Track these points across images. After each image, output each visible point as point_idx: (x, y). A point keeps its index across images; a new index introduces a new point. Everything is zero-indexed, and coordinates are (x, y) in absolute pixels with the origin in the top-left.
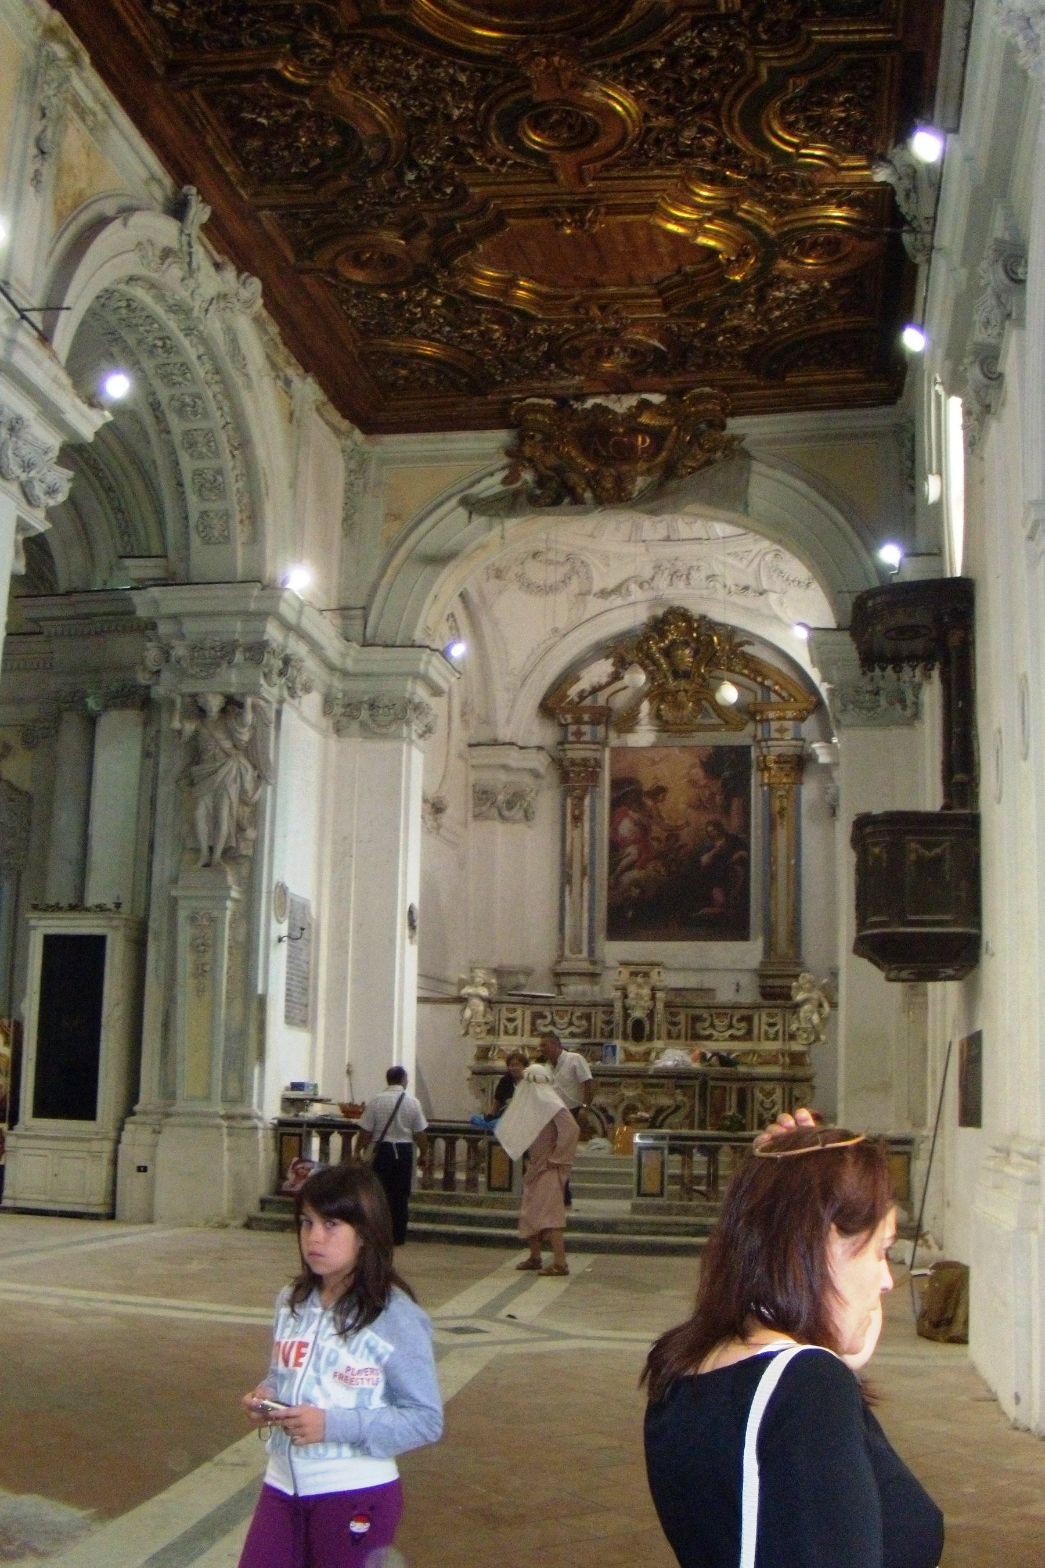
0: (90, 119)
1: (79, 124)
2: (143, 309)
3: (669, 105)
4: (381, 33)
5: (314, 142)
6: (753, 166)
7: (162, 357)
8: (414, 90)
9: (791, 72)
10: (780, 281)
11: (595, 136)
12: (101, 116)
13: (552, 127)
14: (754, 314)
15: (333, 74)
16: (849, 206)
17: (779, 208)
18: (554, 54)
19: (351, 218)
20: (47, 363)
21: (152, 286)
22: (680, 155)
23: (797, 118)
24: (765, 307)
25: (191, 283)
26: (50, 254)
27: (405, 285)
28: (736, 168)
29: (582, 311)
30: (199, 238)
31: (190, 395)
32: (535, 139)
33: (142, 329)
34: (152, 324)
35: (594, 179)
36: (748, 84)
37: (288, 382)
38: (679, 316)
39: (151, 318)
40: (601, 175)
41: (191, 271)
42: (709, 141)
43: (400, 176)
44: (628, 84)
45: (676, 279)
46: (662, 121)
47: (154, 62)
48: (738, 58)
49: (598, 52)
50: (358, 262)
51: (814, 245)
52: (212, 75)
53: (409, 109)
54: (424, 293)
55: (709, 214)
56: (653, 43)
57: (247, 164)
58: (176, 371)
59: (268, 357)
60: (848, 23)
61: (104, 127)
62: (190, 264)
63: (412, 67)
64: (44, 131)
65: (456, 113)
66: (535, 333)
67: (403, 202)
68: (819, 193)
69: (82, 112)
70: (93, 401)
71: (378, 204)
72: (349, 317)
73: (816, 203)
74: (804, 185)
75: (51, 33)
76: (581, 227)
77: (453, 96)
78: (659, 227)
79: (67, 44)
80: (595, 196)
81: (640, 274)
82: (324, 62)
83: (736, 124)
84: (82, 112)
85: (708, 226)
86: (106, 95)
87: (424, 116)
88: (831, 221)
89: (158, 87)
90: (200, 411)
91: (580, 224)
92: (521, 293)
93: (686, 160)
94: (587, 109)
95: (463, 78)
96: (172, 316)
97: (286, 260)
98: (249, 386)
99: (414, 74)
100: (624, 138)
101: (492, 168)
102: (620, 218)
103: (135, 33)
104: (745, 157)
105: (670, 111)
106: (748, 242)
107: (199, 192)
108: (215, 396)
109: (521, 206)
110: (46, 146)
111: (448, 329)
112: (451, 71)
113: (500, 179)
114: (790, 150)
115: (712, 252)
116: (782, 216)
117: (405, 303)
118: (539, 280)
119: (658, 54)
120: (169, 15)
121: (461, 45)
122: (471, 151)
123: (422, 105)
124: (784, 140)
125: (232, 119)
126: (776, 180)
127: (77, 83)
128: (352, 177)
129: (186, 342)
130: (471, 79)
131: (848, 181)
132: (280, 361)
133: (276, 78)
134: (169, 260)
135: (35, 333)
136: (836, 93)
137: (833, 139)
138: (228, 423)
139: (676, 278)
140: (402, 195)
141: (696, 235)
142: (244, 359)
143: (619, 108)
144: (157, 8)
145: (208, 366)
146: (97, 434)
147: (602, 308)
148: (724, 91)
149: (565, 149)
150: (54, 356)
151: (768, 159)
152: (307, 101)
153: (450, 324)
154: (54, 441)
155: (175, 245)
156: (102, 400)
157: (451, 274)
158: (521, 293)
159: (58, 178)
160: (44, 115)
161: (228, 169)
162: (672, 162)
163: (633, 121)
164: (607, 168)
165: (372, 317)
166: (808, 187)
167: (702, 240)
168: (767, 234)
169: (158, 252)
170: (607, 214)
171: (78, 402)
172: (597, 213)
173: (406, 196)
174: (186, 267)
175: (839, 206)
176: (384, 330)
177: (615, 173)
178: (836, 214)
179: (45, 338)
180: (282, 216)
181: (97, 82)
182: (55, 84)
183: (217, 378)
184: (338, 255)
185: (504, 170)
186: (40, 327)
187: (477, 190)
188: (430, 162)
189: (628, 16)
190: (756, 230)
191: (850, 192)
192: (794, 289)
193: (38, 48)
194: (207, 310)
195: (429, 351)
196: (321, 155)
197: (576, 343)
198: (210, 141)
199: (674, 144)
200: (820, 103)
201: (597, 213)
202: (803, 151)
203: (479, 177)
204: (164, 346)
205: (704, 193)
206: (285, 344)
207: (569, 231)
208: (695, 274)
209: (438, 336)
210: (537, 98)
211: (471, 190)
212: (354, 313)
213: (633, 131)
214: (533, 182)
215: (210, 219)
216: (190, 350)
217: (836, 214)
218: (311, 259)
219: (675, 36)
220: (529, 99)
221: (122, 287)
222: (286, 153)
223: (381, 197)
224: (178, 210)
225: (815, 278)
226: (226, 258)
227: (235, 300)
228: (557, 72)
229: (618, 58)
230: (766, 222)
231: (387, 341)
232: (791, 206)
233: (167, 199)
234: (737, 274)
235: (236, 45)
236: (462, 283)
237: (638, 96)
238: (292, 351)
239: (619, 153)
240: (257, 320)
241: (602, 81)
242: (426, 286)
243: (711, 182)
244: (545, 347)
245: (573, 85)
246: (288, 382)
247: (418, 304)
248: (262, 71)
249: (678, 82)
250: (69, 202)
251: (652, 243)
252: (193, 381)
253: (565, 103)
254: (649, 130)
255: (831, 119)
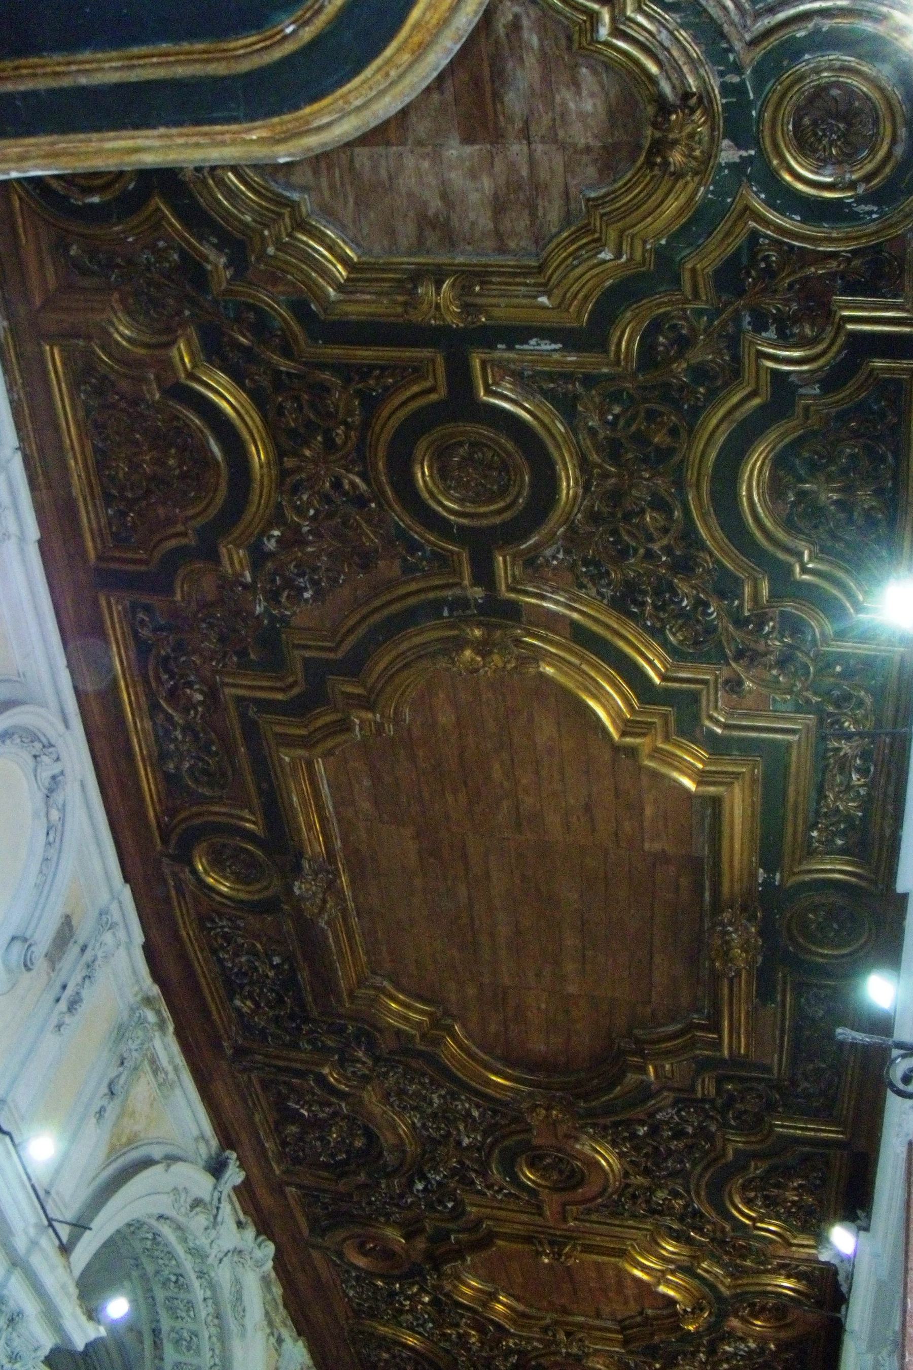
0: (161, 1076)
1: (150, 1076)
2: (166, 1245)
3: (646, 1167)
4: (414, 1064)
5: (343, 1140)
6: (714, 1231)
7: (173, 1290)
8: (434, 1116)
9: (755, 1156)
10: (730, 1336)
11: (581, 1183)
12: (172, 1076)
13: (545, 1168)
14: (706, 1363)
15: (369, 1088)
16: (796, 1278)
17: (737, 1272)
18: (553, 1108)
19: (364, 1210)
20: (61, 1270)
21: (179, 1228)
22: (653, 1212)
23: (756, 1196)
24: (716, 1359)
25: (213, 1233)
26: (94, 1179)
27: (399, 1278)
28: (700, 1230)
29: (550, 1334)
30: (229, 1196)
31: (189, 1331)
32: (529, 1176)
33: (161, 1262)
34: (170, 1260)
35: (575, 1219)
36: (715, 1160)
37: (280, 1341)
38: (637, 1353)
39: (171, 1255)
40: (582, 1217)
41: (215, 1222)
42: (678, 1204)
43: (411, 1184)
44: (614, 1144)
45: (639, 1319)
46: (639, 1180)
47: (225, 1044)
48: (710, 1137)
49: (591, 1114)
50: (361, 1249)
51: (763, 1309)
52: (269, 1066)
53: (427, 1130)
54: (415, 1289)
55: (672, 1267)
56: (639, 1113)
57: (284, 1144)
58: (181, 1306)
59: (267, 1313)
60: (805, 1122)
61: (172, 1086)
62: (216, 1217)
63: (435, 1096)
64: (118, 1076)
65: (466, 1141)
66: (507, 1345)
67: (409, 1207)
68: (771, 1264)
69: (156, 1069)
70: (92, 1314)
71: (388, 1204)
72: (347, 1295)
73: (767, 1271)
74: (757, 1254)
75: (148, 1001)
76: (558, 1260)
77: (466, 1127)
78: (626, 1270)
79: (158, 1012)
80: (575, 1234)
81: (606, 1310)
82: (364, 1076)
83: (703, 1193)
84: (156, 1069)
85: (670, 1277)
86: (180, 1060)
87: (438, 1138)
88: (780, 1290)
89: (224, 1065)
90: (194, 1347)
91: (557, 1255)
92: (499, 1307)
93: (656, 1216)
94: (577, 1159)
95: (476, 1114)
96: (190, 1257)
97: (301, 1233)
98: (243, 1335)
99: (436, 1101)
100: (605, 1190)
101: (489, 1193)
102: (595, 1257)
103: (215, 1016)
104: (709, 1222)
105: (647, 1172)
106: (704, 1298)
107: (238, 1158)
108: (210, 1337)
109: (508, 1231)
110: (117, 1088)
111: (431, 1325)
112: (467, 1105)
113: (496, 1204)
114: (747, 1222)
115: (672, 1302)
116: (736, 1279)
117: (397, 1294)
118: (517, 1299)
119: (642, 1123)
120: (245, 1010)
121: (478, 1086)
122: (474, 1176)
123: (438, 1129)
124: (743, 1213)
125: (280, 1105)
126: (734, 1247)
127: (158, 1043)
128: (369, 1175)
129: (196, 1283)
130: (483, 1115)
131: (796, 1256)
132: (277, 1320)
133: (321, 1080)
134: (198, 1209)
135: (57, 1243)
136: (790, 1178)
137: (786, 1218)
138: (215, 1365)
139: (639, 1319)
140: (409, 1200)
141: (659, 1283)
142: (244, 1311)
143: (603, 1163)
144: (238, 1003)
145: (211, 1310)
146: (87, 1345)
147: (568, 1334)
148: (694, 1164)
149: (555, 1189)
150: (69, 1267)
151: (728, 1228)
152: (343, 1105)
153: (433, 1321)
154: (47, 1342)
155: (207, 1198)
156: (101, 1316)
157: (439, 1277)
158: (499, 1307)
159: (120, 1116)
160: (122, 1063)
161: (267, 1145)
162: (644, 1216)
163: (614, 1175)
164: (589, 1211)
165: (365, 1301)
166: (762, 1258)
167: (662, 1289)
168: (721, 1292)
169: (189, 1201)
170: (582, 1251)
171: (79, 1311)
172: (574, 1248)
173: (412, 1203)
174: (212, 1219)
175: (788, 1277)
176: (373, 1315)
177: (594, 1217)
178: (786, 1284)
179: (65, 1249)
180: (305, 1195)
181: (175, 1048)
182: (139, 1041)
183: (216, 1321)
184: (348, 1238)
185: (500, 1197)
186: (65, 1239)
187: (474, 1209)
188: (438, 1178)
189: (619, 1088)
190: (712, 1287)
191: (798, 1266)
192: (742, 1346)
193: (132, 1010)
194: (221, 1261)
195: (411, 1341)
196: (348, 1152)
197: (542, 1361)
198: (257, 1118)
199: (648, 1202)
200: (778, 1186)
201: (574, 1248)
202: (759, 1225)
203: (478, 1199)
204: (176, 1282)
205: (669, 1247)
206: (286, 1306)
207: (546, 1261)
208: (656, 1318)
209: (421, 1330)
210: (536, 1142)
211: (469, 1209)
212: (351, 1293)
213: (614, 1183)
214: (522, 1212)
215: (243, 1182)
216: (199, 1292)
217: (786, 1284)
218: (322, 1237)
219: (660, 1110)
220: (529, 1142)
221: (153, 1222)
222: (318, 1143)
223: (392, 1198)
224: (216, 1169)
225: (762, 1340)
226: (249, 1220)
227: (248, 1257)
228: (555, 1123)
229: (608, 1121)
230: (722, 1282)
231: (376, 1325)
232: (745, 1271)
233: (211, 1157)
234: (691, 1324)
235: (295, 1046)
236: (448, 1288)
237: (621, 1155)
238: (290, 1313)
239: (600, 1200)
240: (265, 1280)
241: (592, 1137)
242: (417, 1283)
243: (677, 1239)
244: (514, 1359)
245: (567, 1136)
246: (280, 1341)
247: (408, 1298)
248: (311, 1072)
249: (656, 1149)
250: (124, 1140)
251: (620, 1283)
252: (195, 1318)
253: (559, 1150)
254: (628, 1186)
255: (786, 1200)
